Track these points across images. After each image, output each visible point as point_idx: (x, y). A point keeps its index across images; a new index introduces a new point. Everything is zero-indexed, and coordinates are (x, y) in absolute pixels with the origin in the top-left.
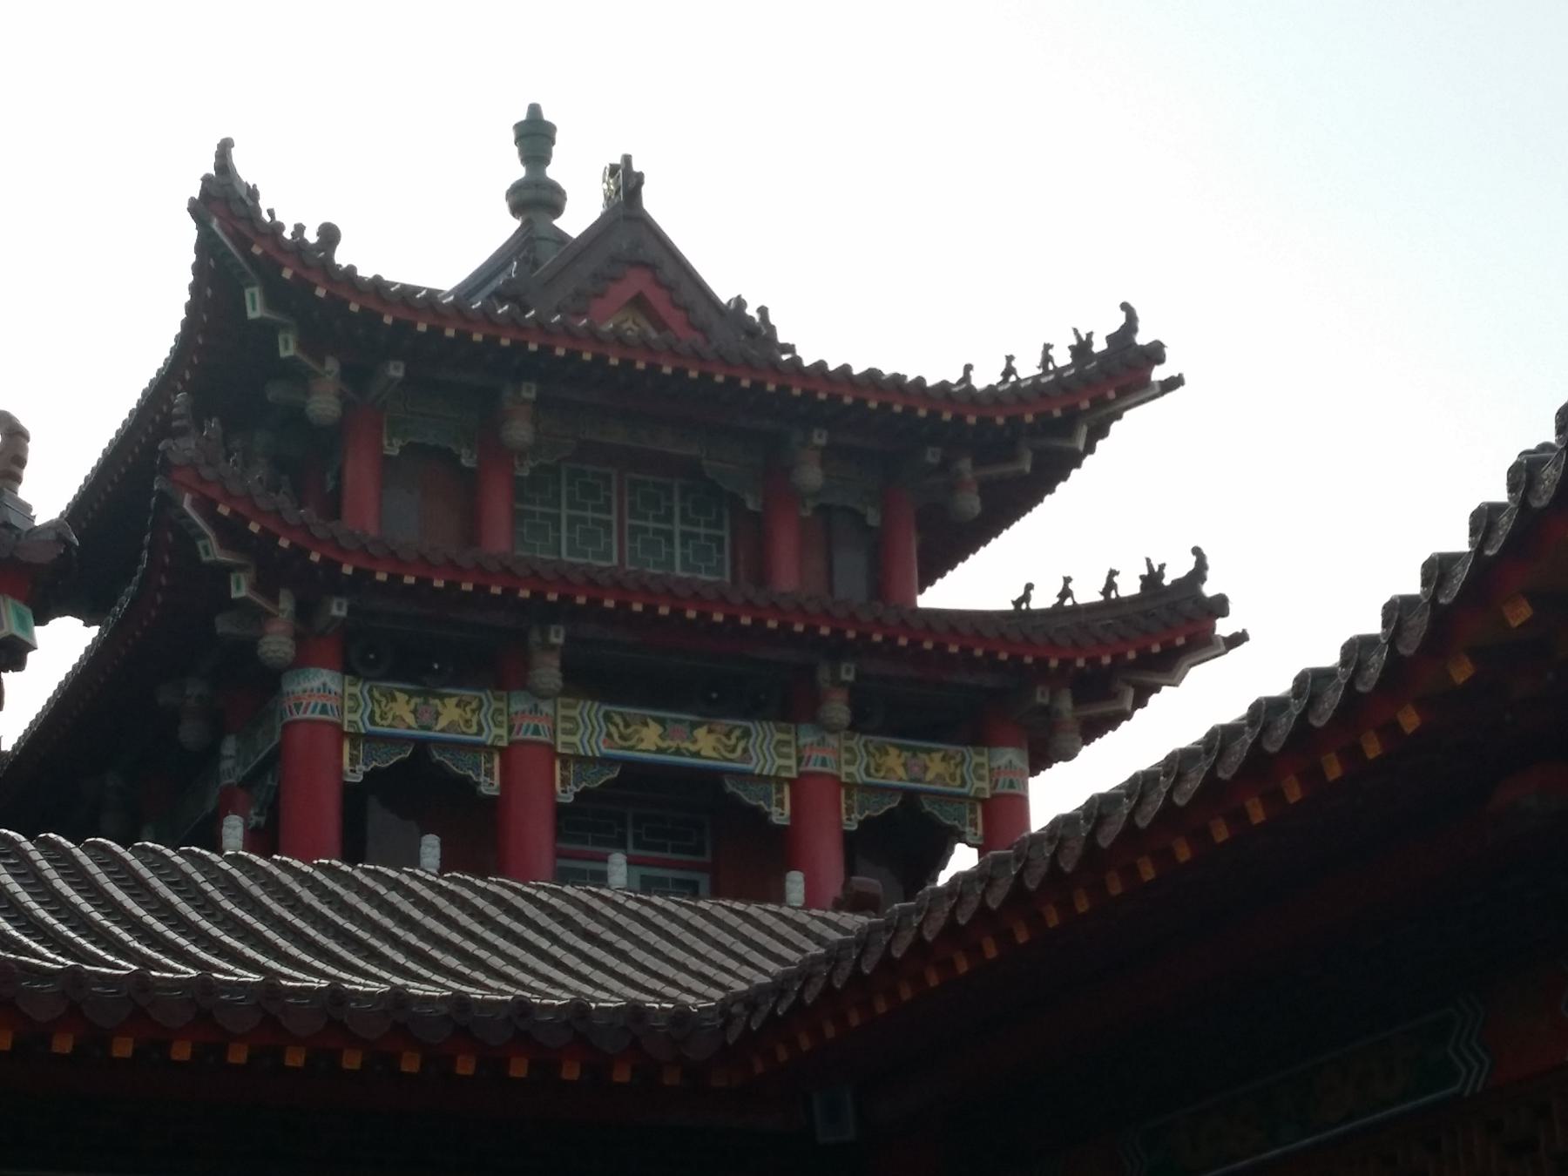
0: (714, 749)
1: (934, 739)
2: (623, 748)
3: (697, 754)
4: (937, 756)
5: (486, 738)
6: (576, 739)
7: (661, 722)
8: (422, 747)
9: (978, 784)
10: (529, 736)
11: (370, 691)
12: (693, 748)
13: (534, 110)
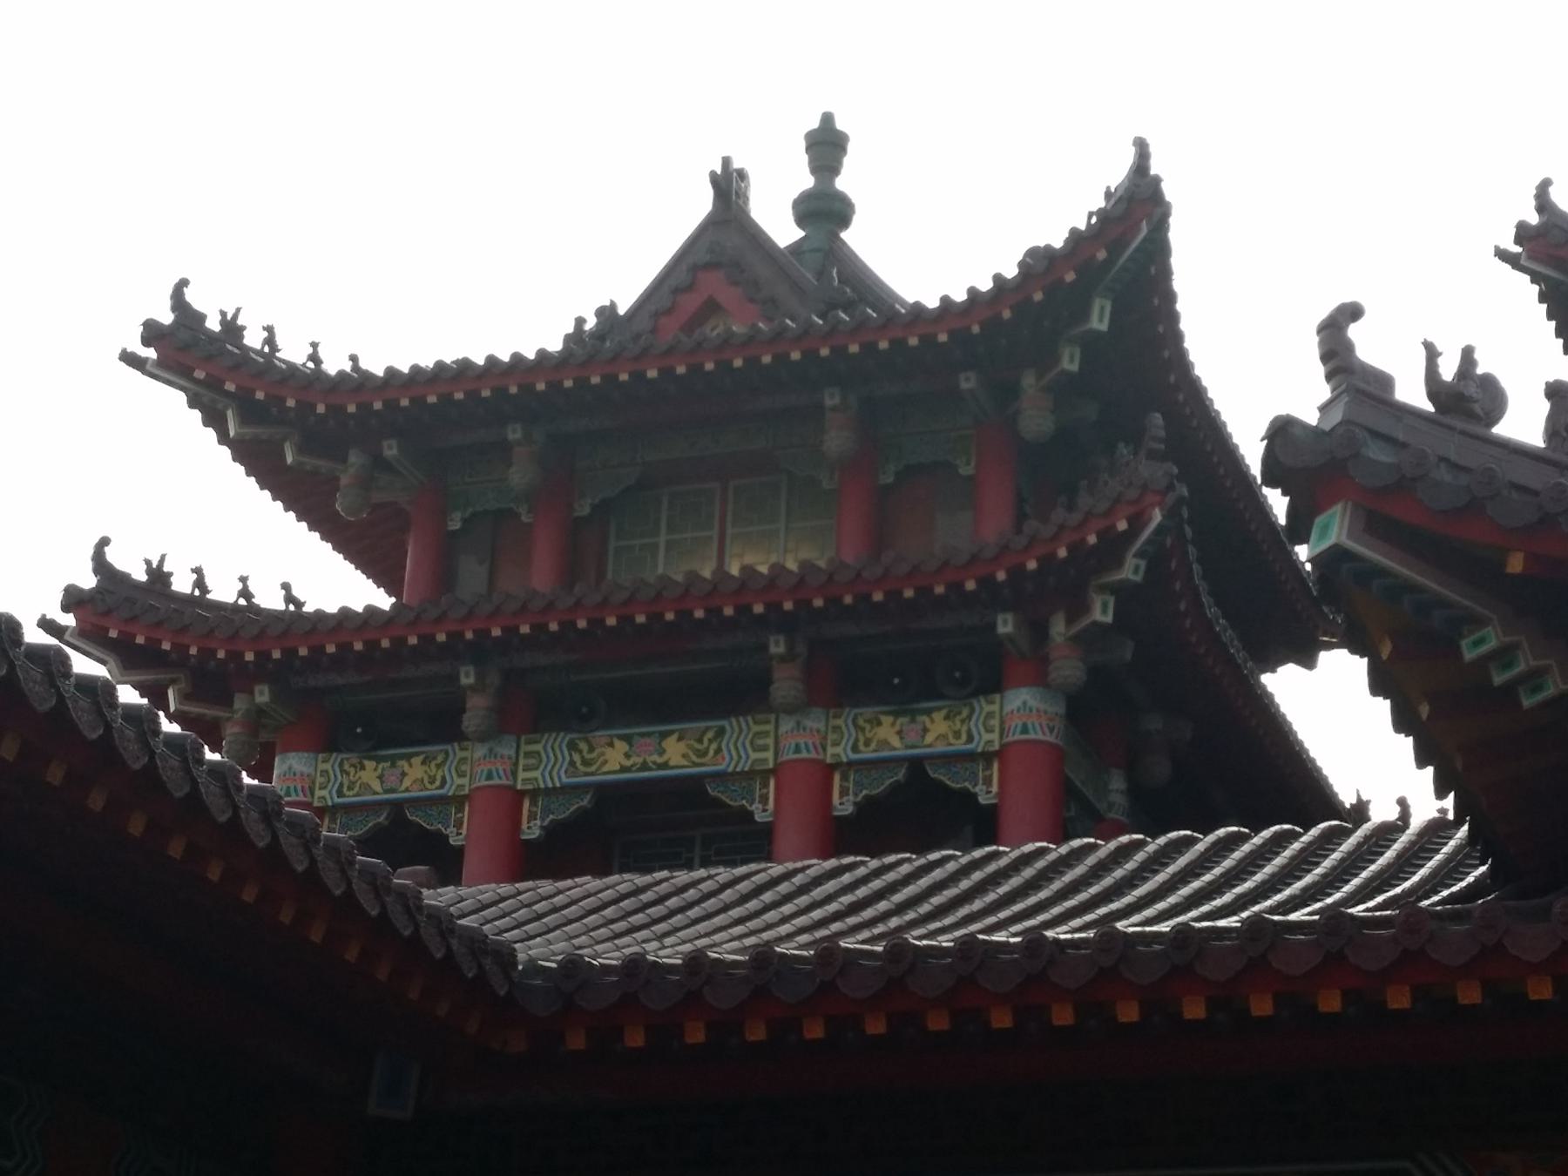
0: (684, 756)
1: (412, 744)
2: (587, 774)
3: (665, 766)
4: (417, 761)
5: (978, 746)
6: (536, 774)
7: (627, 739)
8: (916, 765)
9: (987, 737)
10: (1018, 737)
11: (341, 765)
12: (660, 760)
13: (827, 119)
